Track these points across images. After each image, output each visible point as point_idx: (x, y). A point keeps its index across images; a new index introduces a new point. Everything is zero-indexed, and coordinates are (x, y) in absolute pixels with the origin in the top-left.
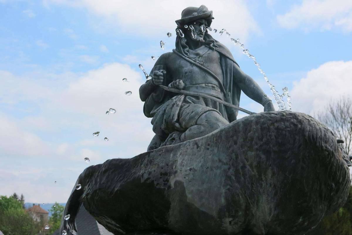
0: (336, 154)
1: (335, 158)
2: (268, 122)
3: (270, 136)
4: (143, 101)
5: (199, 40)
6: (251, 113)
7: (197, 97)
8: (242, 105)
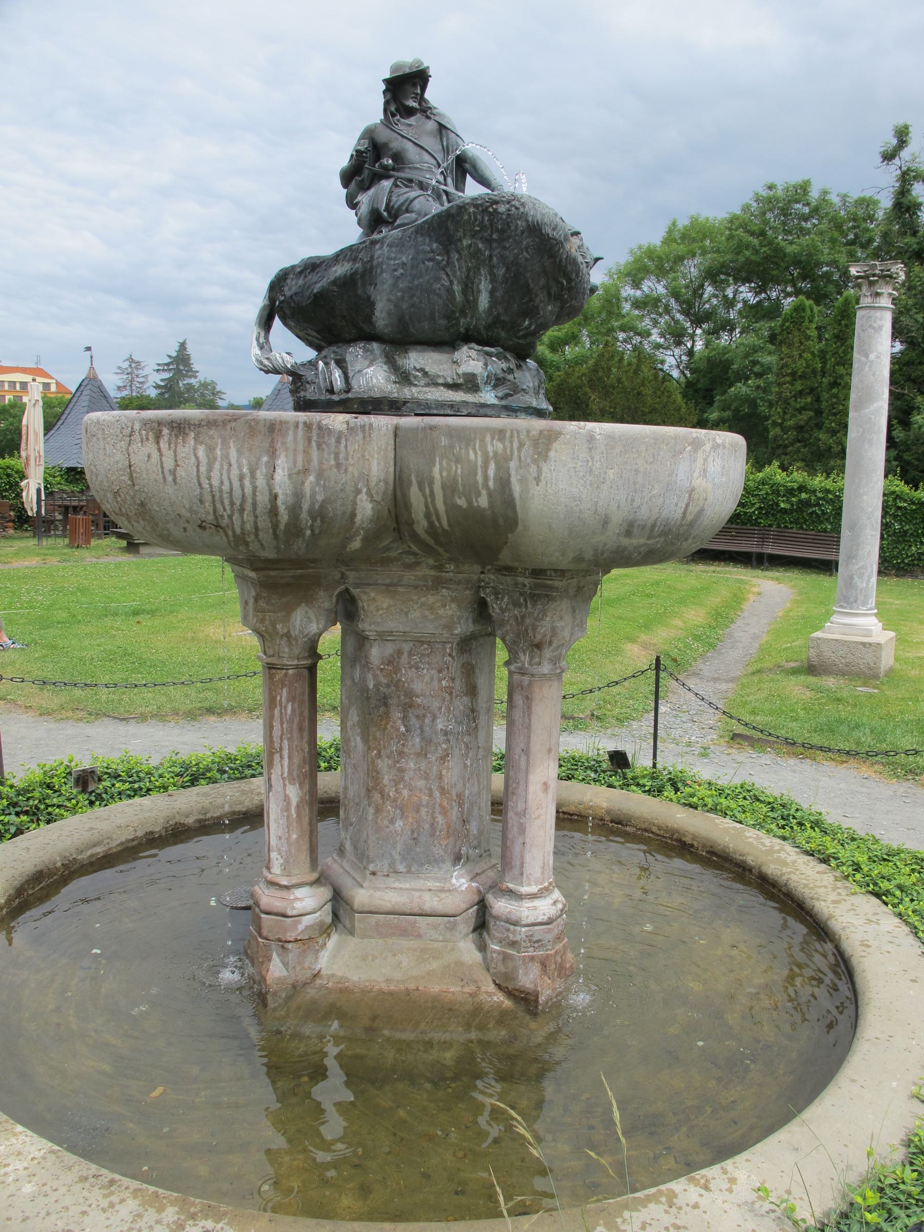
7: (411, 181)
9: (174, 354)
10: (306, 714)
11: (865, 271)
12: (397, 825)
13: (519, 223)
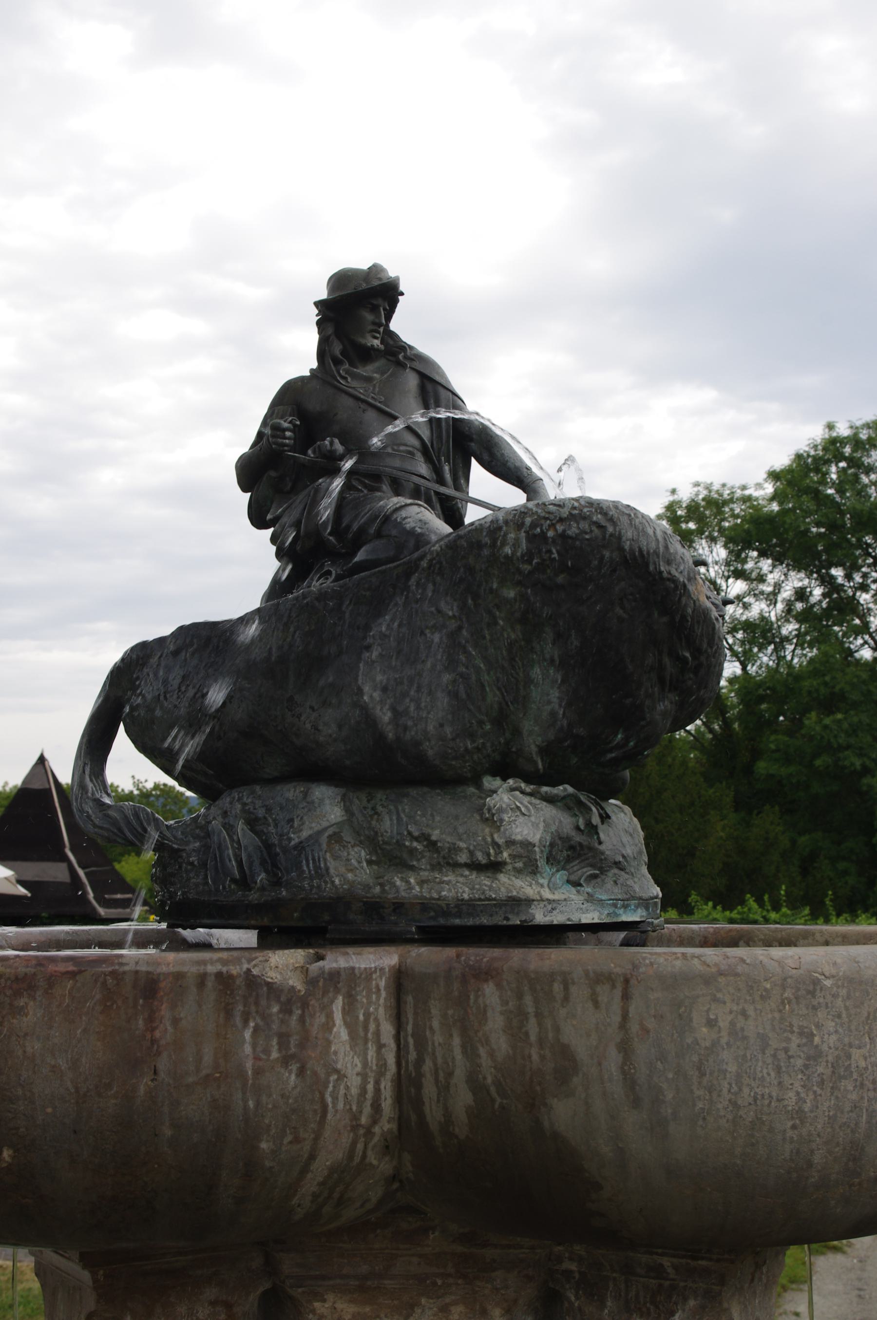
0: (691, 588)
1: (689, 596)
2: (543, 522)
3: (549, 552)
4: (244, 490)
5: (372, 346)
6: (496, 509)
8: (474, 491)
13: (607, 554)
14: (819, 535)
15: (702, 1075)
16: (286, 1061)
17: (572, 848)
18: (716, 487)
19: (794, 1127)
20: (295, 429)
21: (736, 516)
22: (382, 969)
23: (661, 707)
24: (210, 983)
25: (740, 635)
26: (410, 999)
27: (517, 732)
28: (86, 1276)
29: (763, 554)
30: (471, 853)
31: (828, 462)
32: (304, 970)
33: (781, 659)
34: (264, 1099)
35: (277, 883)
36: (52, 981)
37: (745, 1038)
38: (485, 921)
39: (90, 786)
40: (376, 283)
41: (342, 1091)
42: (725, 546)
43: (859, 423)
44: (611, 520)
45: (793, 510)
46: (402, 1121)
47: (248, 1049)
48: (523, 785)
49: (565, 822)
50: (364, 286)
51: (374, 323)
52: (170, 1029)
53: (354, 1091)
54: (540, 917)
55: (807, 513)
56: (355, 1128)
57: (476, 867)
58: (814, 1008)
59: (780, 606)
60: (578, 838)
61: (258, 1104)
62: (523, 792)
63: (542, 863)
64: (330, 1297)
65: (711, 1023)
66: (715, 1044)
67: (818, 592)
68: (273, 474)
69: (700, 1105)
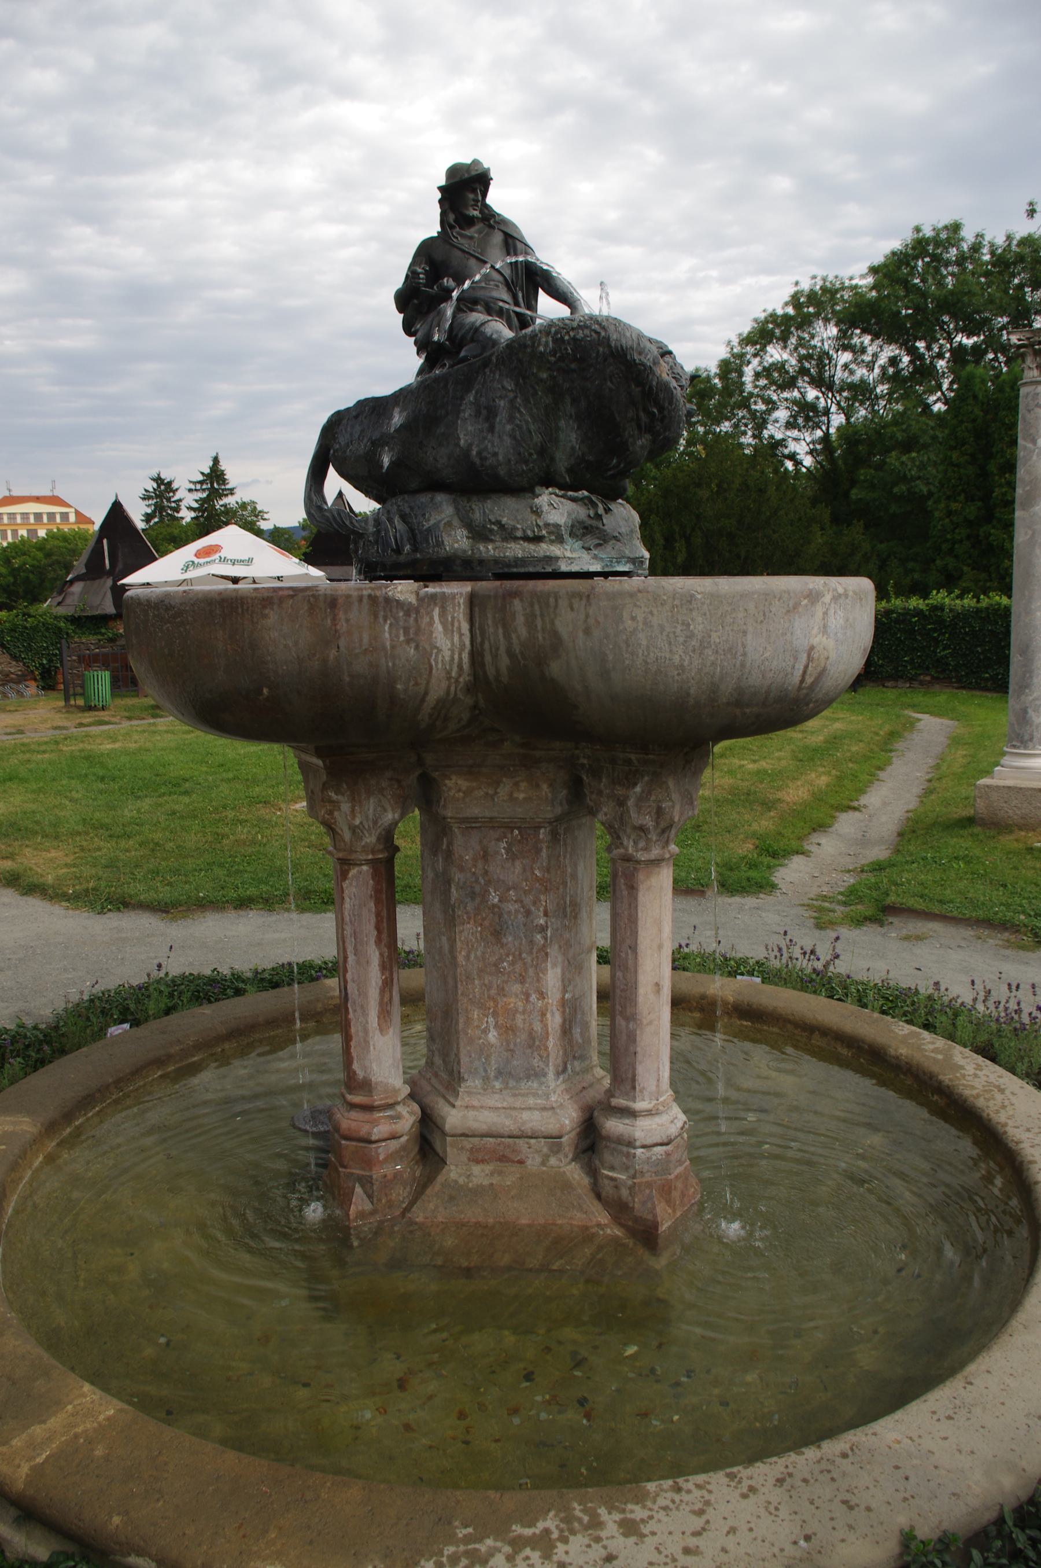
3: (566, 349)
4: (400, 312)
9: (207, 471)
10: (384, 913)
11: (1028, 339)
12: (490, 1035)
13: (601, 349)
14: (907, 315)
15: (628, 646)
16: (408, 641)
17: (586, 528)
18: (831, 278)
19: (679, 674)
20: (426, 273)
21: (846, 302)
22: (461, 594)
23: (639, 443)
24: (365, 600)
25: (845, 394)
26: (477, 609)
27: (552, 459)
28: (320, 763)
29: (864, 331)
30: (524, 531)
31: (916, 258)
32: (417, 594)
33: (875, 412)
34: (397, 662)
35: (415, 549)
36: (281, 600)
37: (651, 626)
38: (531, 569)
39: (315, 498)
40: (473, 173)
41: (440, 658)
42: (836, 325)
43: (940, 226)
44: (604, 328)
45: (888, 296)
46: (475, 675)
47: (387, 635)
48: (557, 491)
49: (581, 512)
50: (466, 176)
51: (474, 200)
52: (345, 625)
53: (447, 659)
54: (564, 567)
55: (898, 298)
56: (449, 678)
57: (526, 539)
58: (691, 610)
59: (877, 371)
60: (589, 522)
61: (394, 664)
62: (557, 495)
63: (566, 537)
64: (454, 777)
65: (633, 619)
66: (635, 629)
67: (906, 359)
68: (416, 301)
69: (627, 662)
